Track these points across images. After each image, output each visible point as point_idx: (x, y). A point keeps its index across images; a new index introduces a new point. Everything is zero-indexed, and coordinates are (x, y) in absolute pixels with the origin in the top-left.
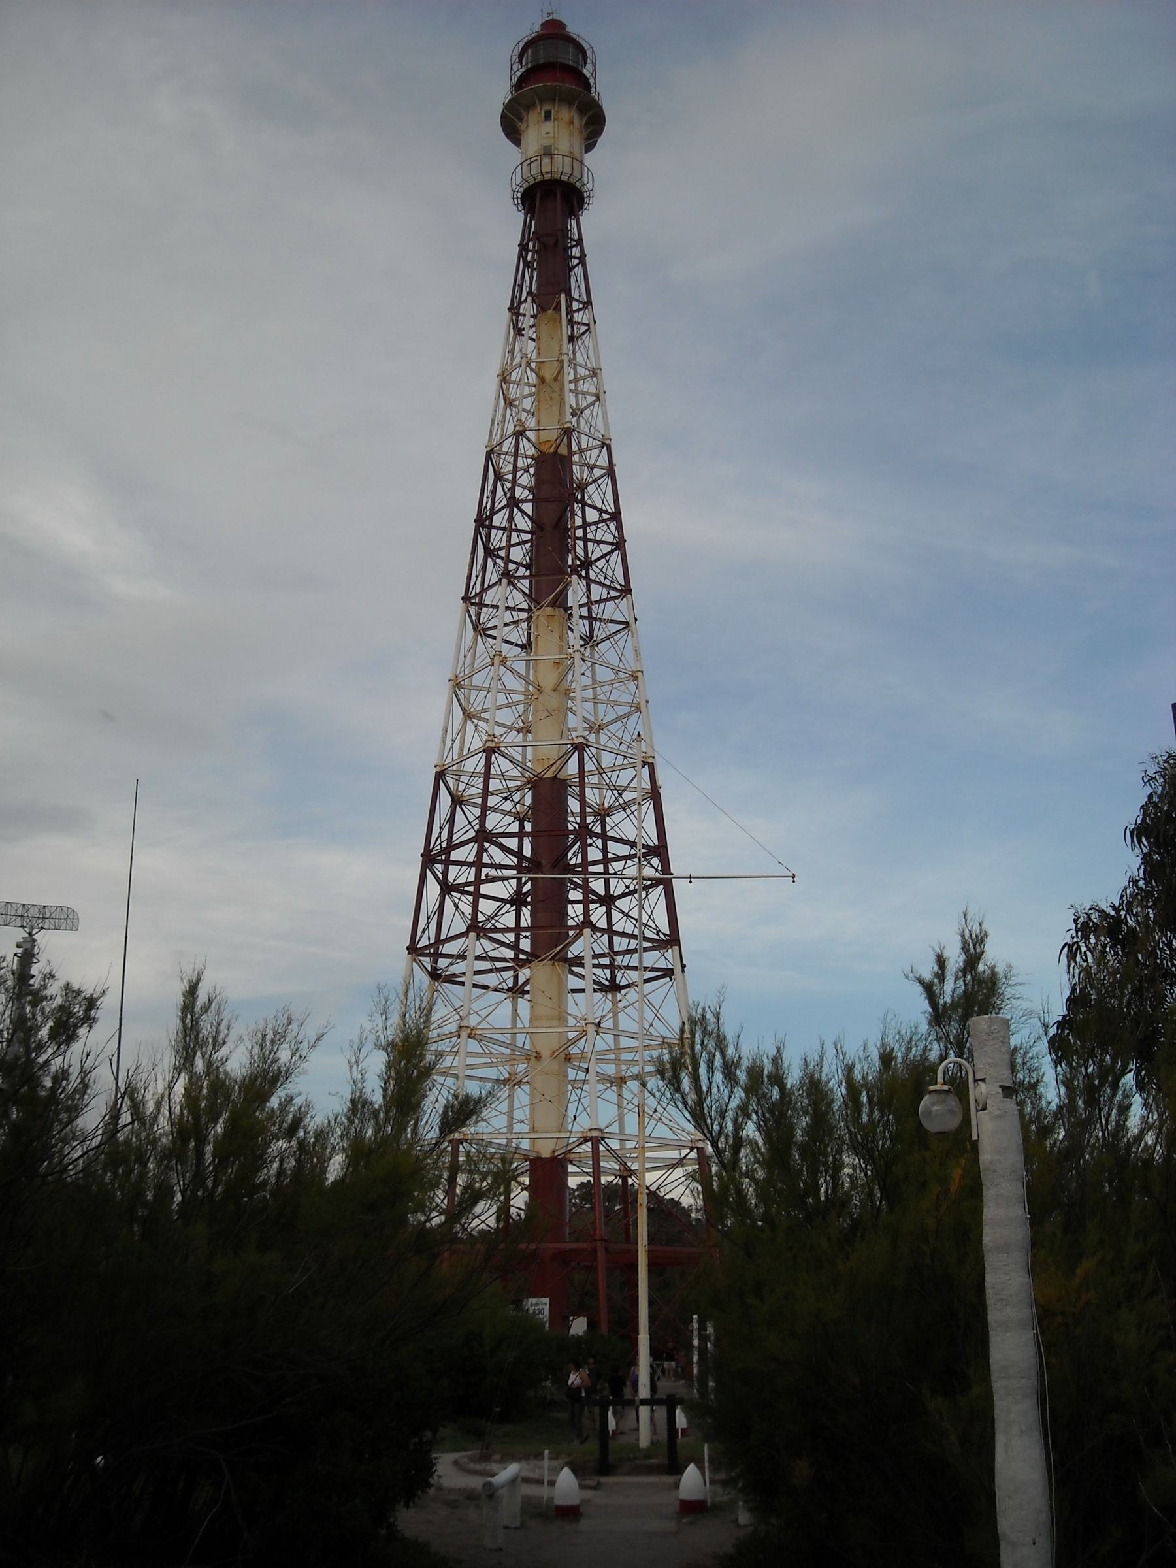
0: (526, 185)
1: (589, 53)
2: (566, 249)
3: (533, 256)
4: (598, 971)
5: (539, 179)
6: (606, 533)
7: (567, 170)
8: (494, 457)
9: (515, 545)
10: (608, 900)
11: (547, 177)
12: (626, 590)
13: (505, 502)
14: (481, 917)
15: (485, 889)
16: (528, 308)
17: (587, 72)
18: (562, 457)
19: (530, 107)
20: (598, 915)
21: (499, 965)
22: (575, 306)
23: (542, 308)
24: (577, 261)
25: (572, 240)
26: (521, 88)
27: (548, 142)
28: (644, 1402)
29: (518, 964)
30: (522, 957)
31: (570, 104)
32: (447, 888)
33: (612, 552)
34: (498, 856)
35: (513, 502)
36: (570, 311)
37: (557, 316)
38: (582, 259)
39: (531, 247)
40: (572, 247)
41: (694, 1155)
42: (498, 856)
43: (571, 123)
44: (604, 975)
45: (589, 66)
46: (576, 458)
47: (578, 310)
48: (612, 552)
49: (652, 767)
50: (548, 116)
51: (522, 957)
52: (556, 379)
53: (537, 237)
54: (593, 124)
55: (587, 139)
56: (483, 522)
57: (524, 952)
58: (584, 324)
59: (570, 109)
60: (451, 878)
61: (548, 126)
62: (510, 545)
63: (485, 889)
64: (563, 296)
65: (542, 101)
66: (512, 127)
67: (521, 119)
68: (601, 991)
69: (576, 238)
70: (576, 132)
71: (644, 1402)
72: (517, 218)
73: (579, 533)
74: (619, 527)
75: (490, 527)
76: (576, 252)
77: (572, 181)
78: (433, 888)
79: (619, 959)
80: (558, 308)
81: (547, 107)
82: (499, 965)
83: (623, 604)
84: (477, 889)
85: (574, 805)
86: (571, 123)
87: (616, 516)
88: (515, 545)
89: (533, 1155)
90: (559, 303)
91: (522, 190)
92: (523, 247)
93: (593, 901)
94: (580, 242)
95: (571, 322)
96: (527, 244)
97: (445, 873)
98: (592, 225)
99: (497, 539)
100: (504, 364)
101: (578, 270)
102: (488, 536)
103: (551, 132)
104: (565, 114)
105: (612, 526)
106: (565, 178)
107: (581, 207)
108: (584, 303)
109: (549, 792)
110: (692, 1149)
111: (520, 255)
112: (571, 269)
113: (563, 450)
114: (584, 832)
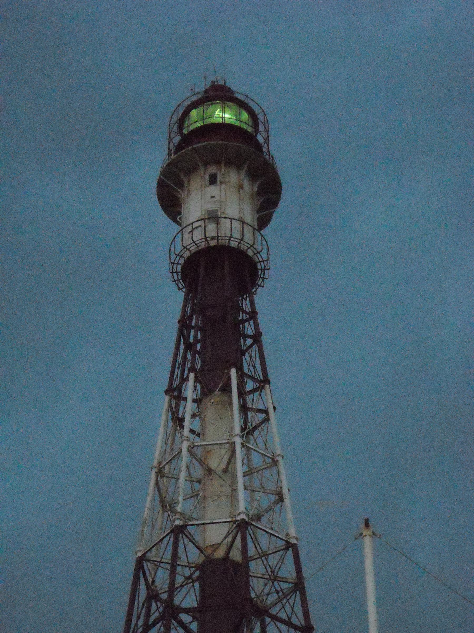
0: (187, 254)
2: (237, 324)
3: (196, 335)
5: (203, 245)
7: (237, 235)
8: (148, 566)
16: (190, 390)
17: (260, 139)
18: (236, 565)
19: (191, 171)
22: (250, 385)
23: (206, 391)
24: (249, 341)
25: (244, 312)
26: (183, 148)
27: (214, 207)
28: (193, 328)
31: (239, 168)
36: (242, 394)
37: (225, 398)
38: (257, 338)
40: (243, 321)
43: (241, 187)
47: (251, 392)
50: (213, 180)
52: (225, 471)
53: (201, 309)
54: (268, 192)
58: (260, 411)
59: (239, 173)
61: (214, 190)
64: (233, 372)
65: (206, 164)
66: (170, 200)
67: (181, 185)
68: (173, 414)
69: (248, 309)
70: (247, 199)
71: (193, 328)
76: (249, 329)
77: (243, 248)
80: (226, 389)
81: (212, 170)
86: (241, 187)
90: (229, 379)
91: (182, 261)
92: (184, 324)
95: (244, 409)
96: (190, 318)
103: (217, 204)
104: (233, 177)
106: (234, 244)
107: (254, 284)
108: (260, 381)
111: (181, 333)
113: (236, 555)
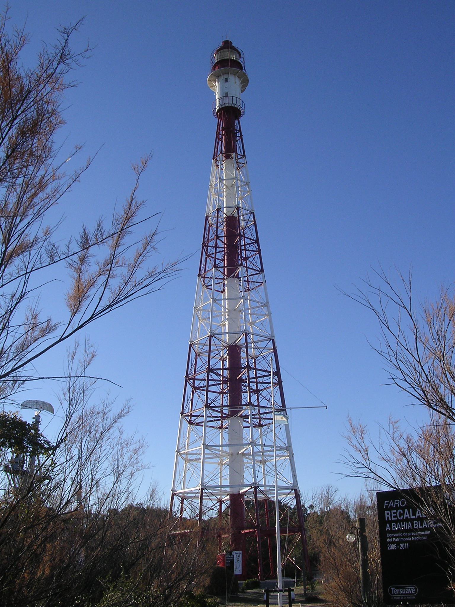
1: (242, 55)
4: (255, 420)
6: (254, 247)
9: (218, 252)
10: (257, 391)
11: (227, 105)
12: (262, 271)
13: (213, 236)
14: (209, 402)
15: (210, 388)
20: (254, 397)
21: (216, 419)
29: (223, 418)
30: (224, 415)
32: (195, 388)
33: (255, 254)
34: (215, 377)
35: (217, 237)
38: (241, 137)
39: (221, 133)
41: (293, 491)
42: (215, 377)
44: (256, 422)
45: (242, 59)
46: (242, 218)
48: (255, 254)
49: (273, 341)
51: (224, 415)
55: (242, 88)
56: (205, 245)
57: (225, 414)
60: (196, 385)
62: (216, 253)
63: (210, 388)
69: (238, 129)
72: (216, 120)
73: (243, 248)
74: (258, 245)
75: (208, 246)
78: (189, 389)
79: (262, 416)
82: (216, 419)
83: (261, 276)
84: (207, 388)
85: (243, 355)
86: (143, 453)
87: (257, 241)
88: (218, 252)
89: (231, 493)
93: (252, 392)
94: (240, 131)
97: (194, 383)
98: (245, 123)
99: (211, 251)
100: (99, 278)
101: (239, 142)
102: (207, 249)
105: (256, 245)
109: (234, 351)
110: (292, 490)
112: (237, 141)
113: (236, 215)
114: (248, 368)
